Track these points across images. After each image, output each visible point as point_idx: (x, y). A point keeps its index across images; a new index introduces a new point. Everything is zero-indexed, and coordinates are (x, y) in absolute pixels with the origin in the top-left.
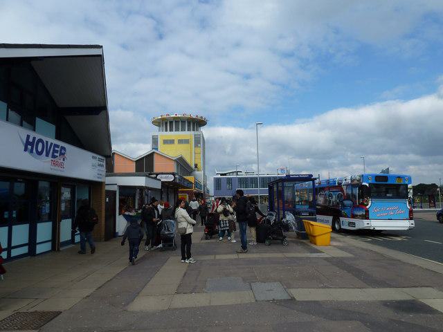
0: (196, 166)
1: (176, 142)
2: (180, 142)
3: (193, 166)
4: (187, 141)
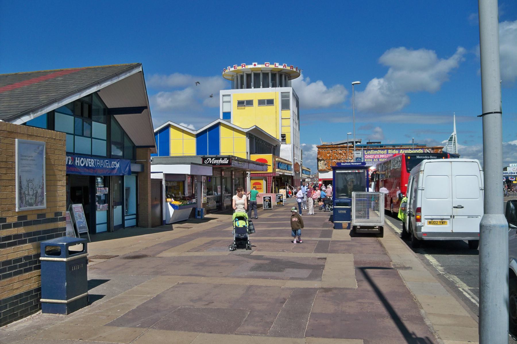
0: (283, 136)
1: (255, 103)
2: (261, 102)
3: (280, 139)
4: (270, 102)
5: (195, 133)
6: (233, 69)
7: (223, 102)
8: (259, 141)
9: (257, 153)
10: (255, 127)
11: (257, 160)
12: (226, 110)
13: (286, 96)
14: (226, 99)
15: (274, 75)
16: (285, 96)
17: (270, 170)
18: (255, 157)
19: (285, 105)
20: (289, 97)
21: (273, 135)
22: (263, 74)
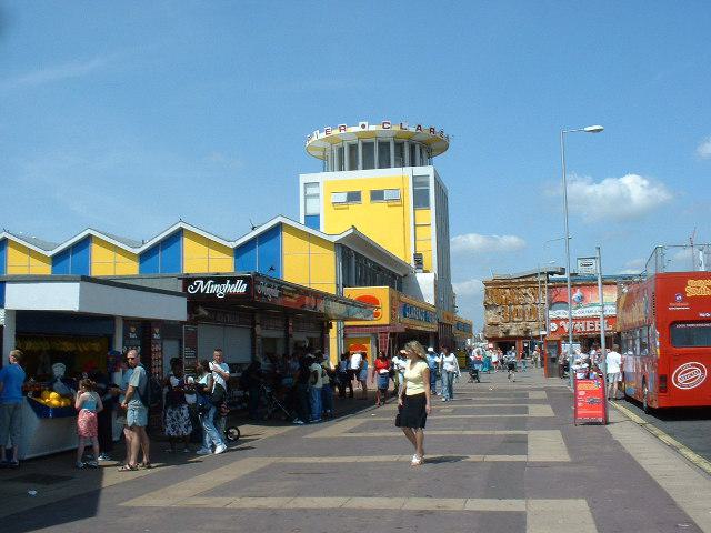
0: (419, 259)
1: (366, 197)
2: (377, 195)
3: (413, 264)
5: (233, 245)
6: (323, 135)
7: (306, 197)
8: (360, 260)
9: (361, 283)
10: (351, 231)
11: (358, 299)
12: (311, 211)
13: (422, 184)
14: (311, 191)
15: (399, 146)
16: (419, 183)
17: (385, 319)
18: (354, 293)
19: (420, 200)
20: (427, 184)
21: (400, 255)
22: (381, 144)
